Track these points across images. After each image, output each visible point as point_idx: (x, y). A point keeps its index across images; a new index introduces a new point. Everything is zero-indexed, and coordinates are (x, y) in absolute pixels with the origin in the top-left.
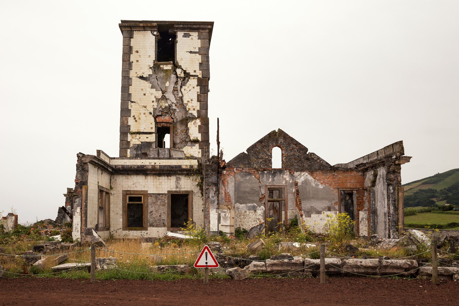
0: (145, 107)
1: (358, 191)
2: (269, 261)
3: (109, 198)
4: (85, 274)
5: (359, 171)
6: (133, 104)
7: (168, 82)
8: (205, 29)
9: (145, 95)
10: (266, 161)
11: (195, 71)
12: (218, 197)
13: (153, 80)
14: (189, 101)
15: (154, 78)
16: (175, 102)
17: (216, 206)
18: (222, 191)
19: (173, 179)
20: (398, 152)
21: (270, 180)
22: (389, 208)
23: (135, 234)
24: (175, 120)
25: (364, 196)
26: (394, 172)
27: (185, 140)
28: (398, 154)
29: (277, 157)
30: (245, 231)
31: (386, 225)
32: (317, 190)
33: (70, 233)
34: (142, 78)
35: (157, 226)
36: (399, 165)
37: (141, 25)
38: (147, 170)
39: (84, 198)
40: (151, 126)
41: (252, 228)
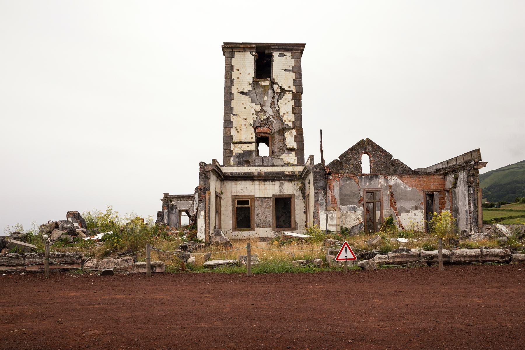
0: (246, 119)
1: (440, 192)
2: (390, 254)
3: (220, 202)
4: (236, 269)
5: (441, 175)
6: (234, 117)
7: (266, 97)
8: (296, 50)
9: (245, 108)
10: (356, 167)
11: (289, 87)
12: (326, 200)
13: (252, 95)
14: (285, 114)
15: (253, 93)
16: (272, 114)
17: (325, 208)
18: (329, 194)
19: (277, 184)
20: (476, 158)
21: (368, 183)
22: (470, 207)
23: (245, 234)
24: (273, 131)
25: (445, 196)
26: (473, 175)
27: (282, 148)
28: (476, 160)
29: (365, 163)
30: (347, 230)
31: (467, 221)
32: (406, 192)
33: (195, 235)
34: (242, 93)
35: (263, 227)
36: (477, 169)
37: (242, 46)
38: (254, 176)
39: (207, 203)
40: (251, 136)
41: (353, 227)
